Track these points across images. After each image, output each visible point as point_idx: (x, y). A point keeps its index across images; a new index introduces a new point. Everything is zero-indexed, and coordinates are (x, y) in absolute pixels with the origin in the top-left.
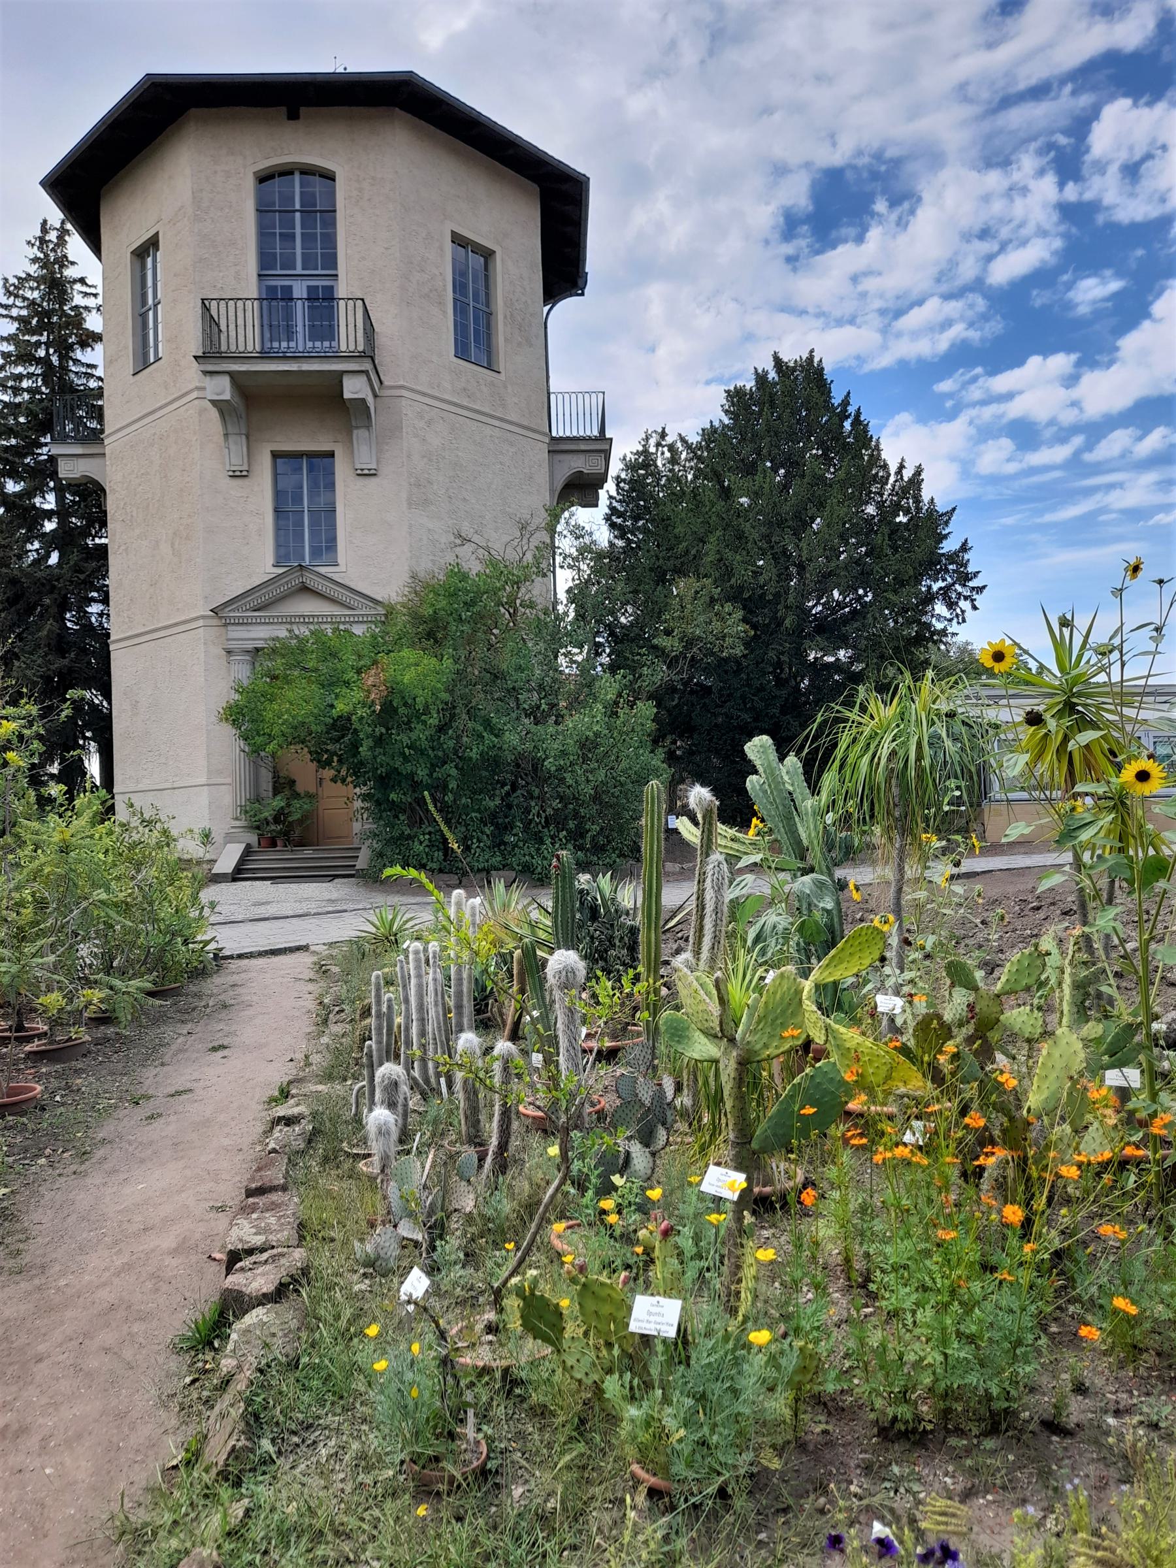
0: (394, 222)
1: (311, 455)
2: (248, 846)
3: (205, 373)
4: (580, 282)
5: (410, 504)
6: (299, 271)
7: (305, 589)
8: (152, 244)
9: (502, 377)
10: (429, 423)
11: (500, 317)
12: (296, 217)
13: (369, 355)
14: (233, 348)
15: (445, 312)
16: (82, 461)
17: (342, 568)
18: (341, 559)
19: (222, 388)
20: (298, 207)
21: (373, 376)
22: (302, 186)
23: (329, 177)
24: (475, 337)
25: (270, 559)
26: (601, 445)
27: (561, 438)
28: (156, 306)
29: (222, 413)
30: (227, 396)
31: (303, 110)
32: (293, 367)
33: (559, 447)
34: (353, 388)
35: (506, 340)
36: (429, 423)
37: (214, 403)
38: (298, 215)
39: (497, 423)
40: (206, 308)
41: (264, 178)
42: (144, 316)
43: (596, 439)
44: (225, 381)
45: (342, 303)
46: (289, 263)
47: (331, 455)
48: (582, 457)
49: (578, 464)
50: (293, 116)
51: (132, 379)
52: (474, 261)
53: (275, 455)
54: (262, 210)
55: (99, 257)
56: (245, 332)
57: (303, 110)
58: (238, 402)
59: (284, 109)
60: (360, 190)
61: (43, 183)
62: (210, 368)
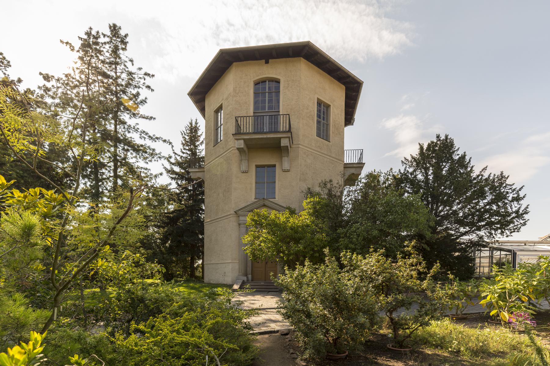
0: (301, 89)
1: (269, 166)
2: (243, 281)
3: (236, 139)
4: (352, 121)
5: (300, 180)
6: (267, 110)
7: (264, 206)
8: (220, 108)
9: (331, 143)
10: (307, 156)
11: (331, 125)
12: (267, 90)
13: (290, 131)
14: (245, 130)
15: (314, 123)
16: (198, 173)
17: (277, 199)
18: (276, 197)
19: (241, 144)
20: (267, 91)
21: (291, 139)
22: (269, 85)
23: (278, 82)
24: (323, 130)
25: (253, 197)
26: (360, 165)
27: (347, 164)
28: (221, 126)
29: (240, 152)
30: (242, 146)
31: (270, 60)
32: (265, 136)
33: (347, 166)
34: (284, 143)
35: (333, 132)
36: (307, 156)
37: (238, 149)
38: (267, 94)
39: (328, 157)
40: (237, 121)
41: (257, 84)
42: (217, 129)
43: (358, 163)
44: (242, 141)
45: (282, 116)
46: (264, 108)
47: (274, 166)
48: (354, 169)
49: (353, 171)
50: (267, 62)
51: (213, 148)
52: (323, 109)
53: (257, 167)
54: (256, 94)
55: (204, 116)
56: (248, 126)
57: (270, 60)
58: (246, 149)
59: (264, 61)
60: (288, 84)
61: (188, 94)
62: (237, 138)
